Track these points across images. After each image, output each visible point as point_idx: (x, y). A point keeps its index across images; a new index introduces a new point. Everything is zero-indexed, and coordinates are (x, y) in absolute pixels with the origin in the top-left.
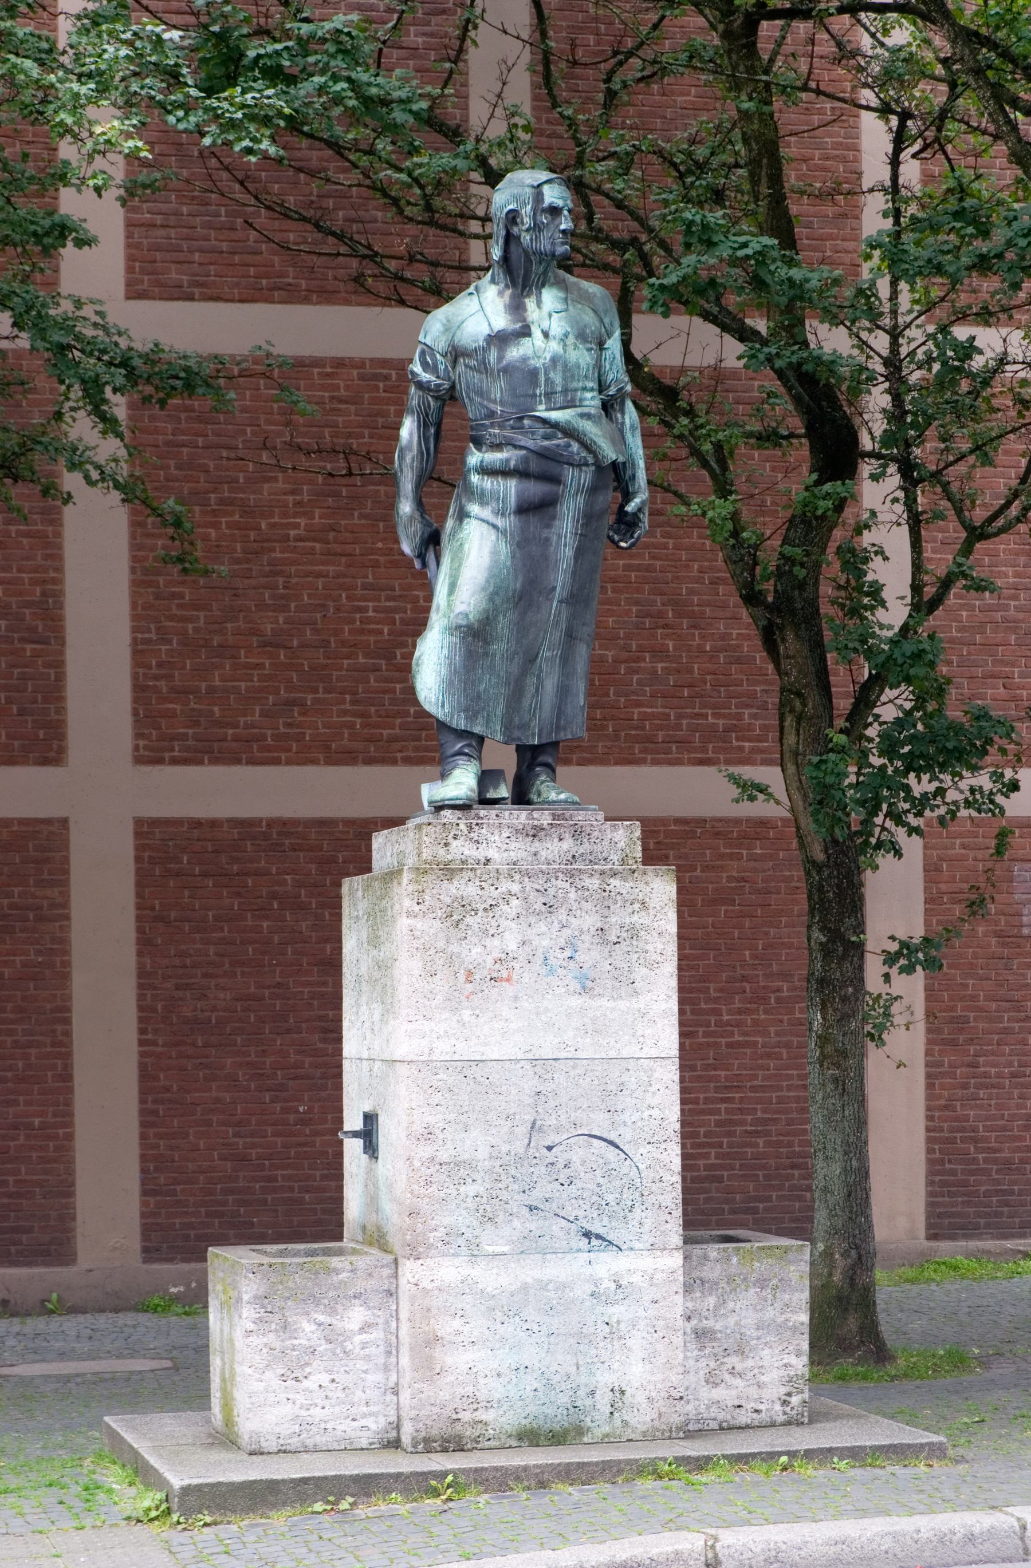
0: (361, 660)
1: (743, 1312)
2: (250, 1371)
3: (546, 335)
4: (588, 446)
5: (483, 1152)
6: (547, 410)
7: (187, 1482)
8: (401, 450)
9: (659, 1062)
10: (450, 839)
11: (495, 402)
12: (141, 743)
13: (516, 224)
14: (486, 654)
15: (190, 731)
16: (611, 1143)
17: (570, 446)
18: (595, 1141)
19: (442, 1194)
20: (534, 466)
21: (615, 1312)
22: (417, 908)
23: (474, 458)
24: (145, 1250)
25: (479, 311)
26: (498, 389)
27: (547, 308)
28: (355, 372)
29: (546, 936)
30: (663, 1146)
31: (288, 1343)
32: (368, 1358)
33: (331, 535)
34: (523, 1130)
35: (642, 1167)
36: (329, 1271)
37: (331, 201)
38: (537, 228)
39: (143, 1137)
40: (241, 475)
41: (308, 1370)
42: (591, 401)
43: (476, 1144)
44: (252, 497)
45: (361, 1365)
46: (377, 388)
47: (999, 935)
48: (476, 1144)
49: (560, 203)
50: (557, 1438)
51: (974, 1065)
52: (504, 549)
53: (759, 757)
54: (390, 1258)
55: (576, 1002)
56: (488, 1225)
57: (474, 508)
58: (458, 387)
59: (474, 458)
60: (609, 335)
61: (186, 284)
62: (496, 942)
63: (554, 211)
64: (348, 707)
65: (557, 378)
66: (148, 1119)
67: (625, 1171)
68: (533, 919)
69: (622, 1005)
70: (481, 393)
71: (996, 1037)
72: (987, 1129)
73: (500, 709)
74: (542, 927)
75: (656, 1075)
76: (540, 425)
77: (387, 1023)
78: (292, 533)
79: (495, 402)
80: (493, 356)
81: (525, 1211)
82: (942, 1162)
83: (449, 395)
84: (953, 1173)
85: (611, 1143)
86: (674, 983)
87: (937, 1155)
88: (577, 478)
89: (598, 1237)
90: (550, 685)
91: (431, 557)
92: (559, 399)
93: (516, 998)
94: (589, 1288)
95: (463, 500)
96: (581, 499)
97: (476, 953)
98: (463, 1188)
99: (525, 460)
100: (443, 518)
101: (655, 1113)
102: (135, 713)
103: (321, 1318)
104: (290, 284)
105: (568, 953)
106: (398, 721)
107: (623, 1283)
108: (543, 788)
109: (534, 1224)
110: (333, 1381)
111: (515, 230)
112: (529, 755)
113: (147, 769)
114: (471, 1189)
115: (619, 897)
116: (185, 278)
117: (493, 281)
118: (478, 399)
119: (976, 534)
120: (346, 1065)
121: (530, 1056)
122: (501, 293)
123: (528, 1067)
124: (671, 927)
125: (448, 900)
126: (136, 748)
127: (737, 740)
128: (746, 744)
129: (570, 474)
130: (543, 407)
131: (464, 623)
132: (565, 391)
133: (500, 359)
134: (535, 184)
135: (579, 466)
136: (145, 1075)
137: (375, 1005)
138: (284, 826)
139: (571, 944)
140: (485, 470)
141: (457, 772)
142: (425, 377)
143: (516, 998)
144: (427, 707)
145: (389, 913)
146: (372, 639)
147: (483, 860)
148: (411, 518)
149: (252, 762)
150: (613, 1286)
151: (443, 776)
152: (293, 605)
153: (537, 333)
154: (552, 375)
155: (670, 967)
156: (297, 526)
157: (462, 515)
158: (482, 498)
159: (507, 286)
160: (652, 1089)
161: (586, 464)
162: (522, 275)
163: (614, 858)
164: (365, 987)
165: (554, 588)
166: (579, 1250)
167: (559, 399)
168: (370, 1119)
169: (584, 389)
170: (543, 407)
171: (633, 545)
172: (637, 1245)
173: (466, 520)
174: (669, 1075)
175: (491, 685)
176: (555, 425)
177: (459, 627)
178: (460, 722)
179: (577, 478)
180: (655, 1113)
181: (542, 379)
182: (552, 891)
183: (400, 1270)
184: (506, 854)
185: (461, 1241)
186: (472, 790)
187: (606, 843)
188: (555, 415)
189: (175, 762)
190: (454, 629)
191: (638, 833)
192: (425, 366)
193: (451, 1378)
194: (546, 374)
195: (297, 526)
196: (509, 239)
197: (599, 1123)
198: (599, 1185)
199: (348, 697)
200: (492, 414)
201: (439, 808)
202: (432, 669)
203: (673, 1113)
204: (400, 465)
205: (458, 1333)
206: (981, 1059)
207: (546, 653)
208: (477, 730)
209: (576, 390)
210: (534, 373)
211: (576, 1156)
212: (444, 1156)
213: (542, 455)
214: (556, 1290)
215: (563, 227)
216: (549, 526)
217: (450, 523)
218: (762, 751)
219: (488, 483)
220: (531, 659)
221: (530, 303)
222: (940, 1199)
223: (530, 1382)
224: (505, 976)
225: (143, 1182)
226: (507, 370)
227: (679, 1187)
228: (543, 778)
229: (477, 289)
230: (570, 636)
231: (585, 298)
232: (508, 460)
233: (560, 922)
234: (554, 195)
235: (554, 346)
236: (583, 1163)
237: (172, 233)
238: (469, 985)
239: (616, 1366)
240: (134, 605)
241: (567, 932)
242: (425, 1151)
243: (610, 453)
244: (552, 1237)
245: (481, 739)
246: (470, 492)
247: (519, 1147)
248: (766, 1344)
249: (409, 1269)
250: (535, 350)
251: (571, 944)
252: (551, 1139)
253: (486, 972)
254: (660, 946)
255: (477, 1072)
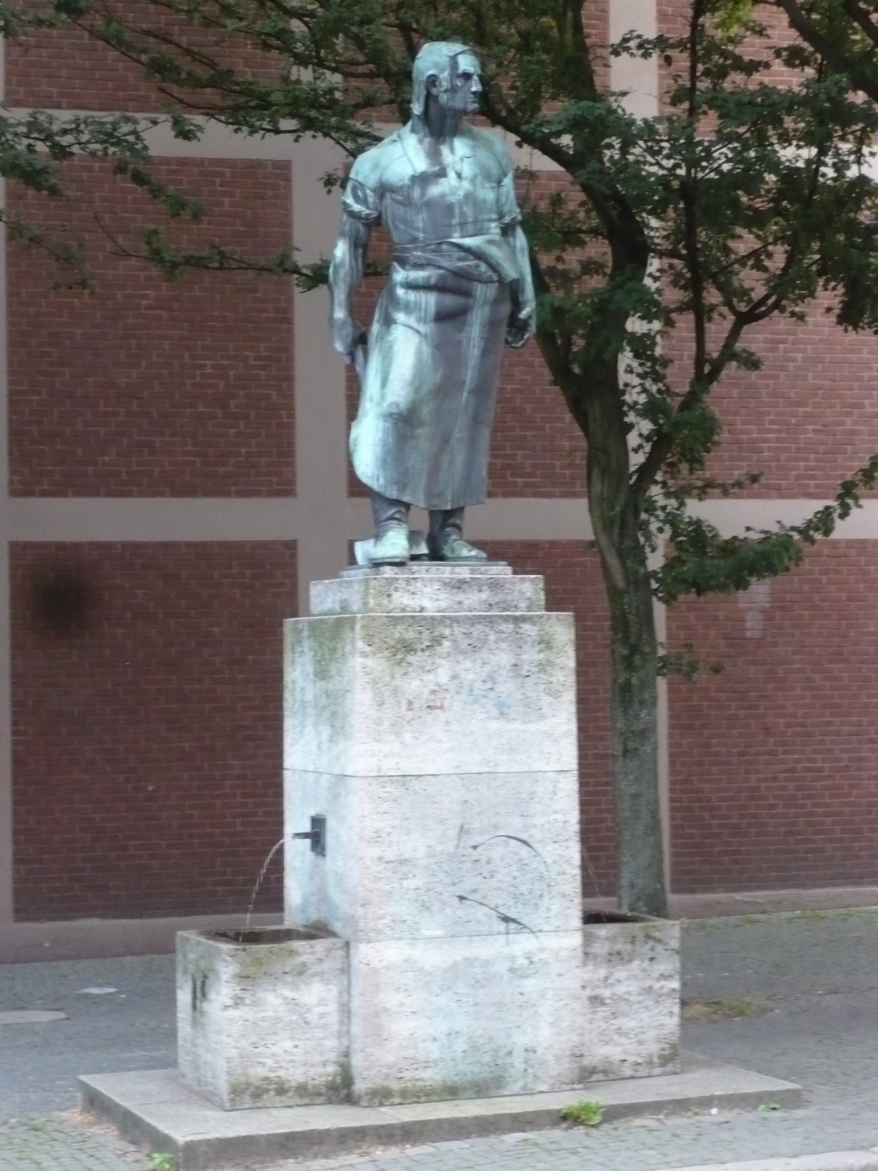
0: (201, 409)
1: (628, 980)
2: (227, 1040)
3: (459, 176)
4: (493, 267)
5: (421, 852)
6: (462, 237)
7: (189, 1138)
8: (335, 267)
9: (563, 775)
10: (392, 592)
11: (417, 229)
12: (16, 478)
13: (435, 86)
14: (413, 437)
15: (57, 468)
16: (525, 842)
17: (477, 266)
18: (511, 840)
19: (388, 888)
20: (450, 282)
21: (530, 985)
22: (368, 649)
23: (400, 275)
24: (17, 911)
25: (399, 156)
26: (420, 220)
27: (459, 154)
28: (196, 170)
29: (471, 671)
30: (566, 844)
31: (260, 1015)
32: (325, 1027)
33: (176, 305)
34: (453, 833)
35: (549, 861)
36: (292, 953)
37: (176, 28)
38: (453, 90)
39: (15, 813)
40: (101, 254)
41: (277, 1038)
42: (494, 229)
43: (416, 845)
44: (110, 272)
45: (318, 1033)
46: (214, 182)
47: (725, 637)
48: (416, 845)
49: (471, 70)
50: (481, 1089)
51: (707, 746)
52: (426, 349)
53: (529, 490)
54: (339, 943)
55: (495, 725)
56: (426, 914)
57: (400, 317)
58: (384, 216)
59: (400, 275)
60: (505, 175)
61: (55, 95)
62: (431, 677)
63: (467, 76)
64: (190, 448)
65: (469, 211)
66: (20, 798)
67: (535, 865)
68: (460, 658)
69: (532, 727)
70: (405, 222)
71: (725, 722)
72: (720, 799)
73: (423, 482)
74: (468, 664)
75: (560, 785)
76: (455, 249)
77: (337, 743)
78: (144, 302)
79: (417, 229)
80: (416, 192)
81: (456, 900)
82: (682, 827)
83: (376, 223)
84: (691, 836)
85: (525, 842)
86: (573, 709)
87: (679, 822)
88: (484, 292)
89: (514, 921)
90: (460, 459)
91: (359, 353)
92: (471, 228)
93: (447, 723)
94: (507, 964)
95: (390, 310)
96: (487, 309)
97: (415, 685)
98: (405, 883)
99: (442, 278)
100: (368, 323)
101: (559, 817)
102: (11, 453)
103: (288, 993)
104: (142, 96)
105: (489, 685)
106: (232, 460)
107: (535, 959)
108: (456, 545)
109: (462, 911)
110: (296, 1046)
111: (434, 91)
112: (440, 519)
113: (21, 500)
114: (411, 883)
115: (529, 639)
116: (55, 90)
117: (413, 131)
118: (402, 227)
119: (743, 320)
120: (287, 776)
121: (458, 771)
122: (420, 141)
123: (457, 780)
124: (572, 663)
125: (392, 642)
126: (11, 482)
127: (512, 476)
128: (519, 480)
129: (479, 289)
130: (457, 235)
131: (395, 411)
132: (475, 222)
133: (423, 194)
134: (452, 54)
135: (486, 282)
136: (18, 761)
137: (323, 728)
138: (135, 548)
139: (492, 678)
140: (411, 286)
141: (391, 534)
142: (357, 207)
143: (447, 723)
144: (364, 480)
145: (339, 652)
146: (210, 391)
147: (418, 609)
148: (344, 323)
149: (110, 494)
150: (526, 962)
151: (378, 537)
152: (144, 363)
153: (452, 175)
154: (465, 209)
155: (569, 697)
156: (146, 297)
157: (388, 322)
158: (408, 308)
159: (425, 136)
160: (556, 797)
161: (492, 282)
162: (440, 126)
163: (523, 605)
164: (310, 711)
165: (464, 382)
166: (499, 933)
167: (471, 228)
168: (318, 823)
169: (491, 220)
170: (457, 235)
171: (524, 345)
172: (546, 927)
173: (394, 326)
174: (570, 785)
175: (417, 460)
176: (467, 250)
177: (391, 415)
178: (393, 493)
179: (484, 292)
180: (559, 817)
181: (457, 211)
182: (475, 634)
183: (352, 952)
184: (436, 604)
185: (404, 927)
186: (404, 549)
187: (516, 593)
188: (468, 242)
189: (44, 494)
190: (389, 416)
191: (541, 585)
192: (356, 198)
193: (396, 1043)
194: (461, 208)
195: (146, 297)
196: (429, 98)
197: (514, 826)
198: (515, 878)
199: (189, 440)
200: (415, 240)
201: (377, 564)
202: (368, 445)
203: (574, 817)
204: (335, 279)
205: (402, 1004)
206: (714, 741)
207: (457, 435)
208: (406, 499)
209: (484, 221)
210: (450, 207)
211: (496, 853)
212: (390, 856)
213: (458, 274)
214: (482, 966)
215: (474, 89)
216: (461, 331)
217: (375, 328)
218: (533, 485)
219: (412, 296)
220: (446, 441)
221: (445, 150)
222: (681, 859)
223: (460, 1045)
224: (438, 704)
225: (16, 852)
226: (428, 204)
227: (579, 878)
228: (454, 537)
229: (399, 137)
230: (476, 421)
231: (488, 144)
232: (429, 278)
233: (482, 659)
234: (467, 63)
235: (466, 185)
236: (502, 859)
237: (44, 52)
238: (410, 713)
239: (529, 1029)
240: (10, 363)
241: (488, 668)
242: (375, 852)
243: (511, 273)
244: (479, 922)
245: (407, 506)
246: (393, 300)
247: (450, 847)
248: (645, 1007)
249: (363, 953)
250: (448, 187)
251: (492, 678)
252: (476, 840)
253: (423, 701)
254: (562, 679)
255: (416, 785)
